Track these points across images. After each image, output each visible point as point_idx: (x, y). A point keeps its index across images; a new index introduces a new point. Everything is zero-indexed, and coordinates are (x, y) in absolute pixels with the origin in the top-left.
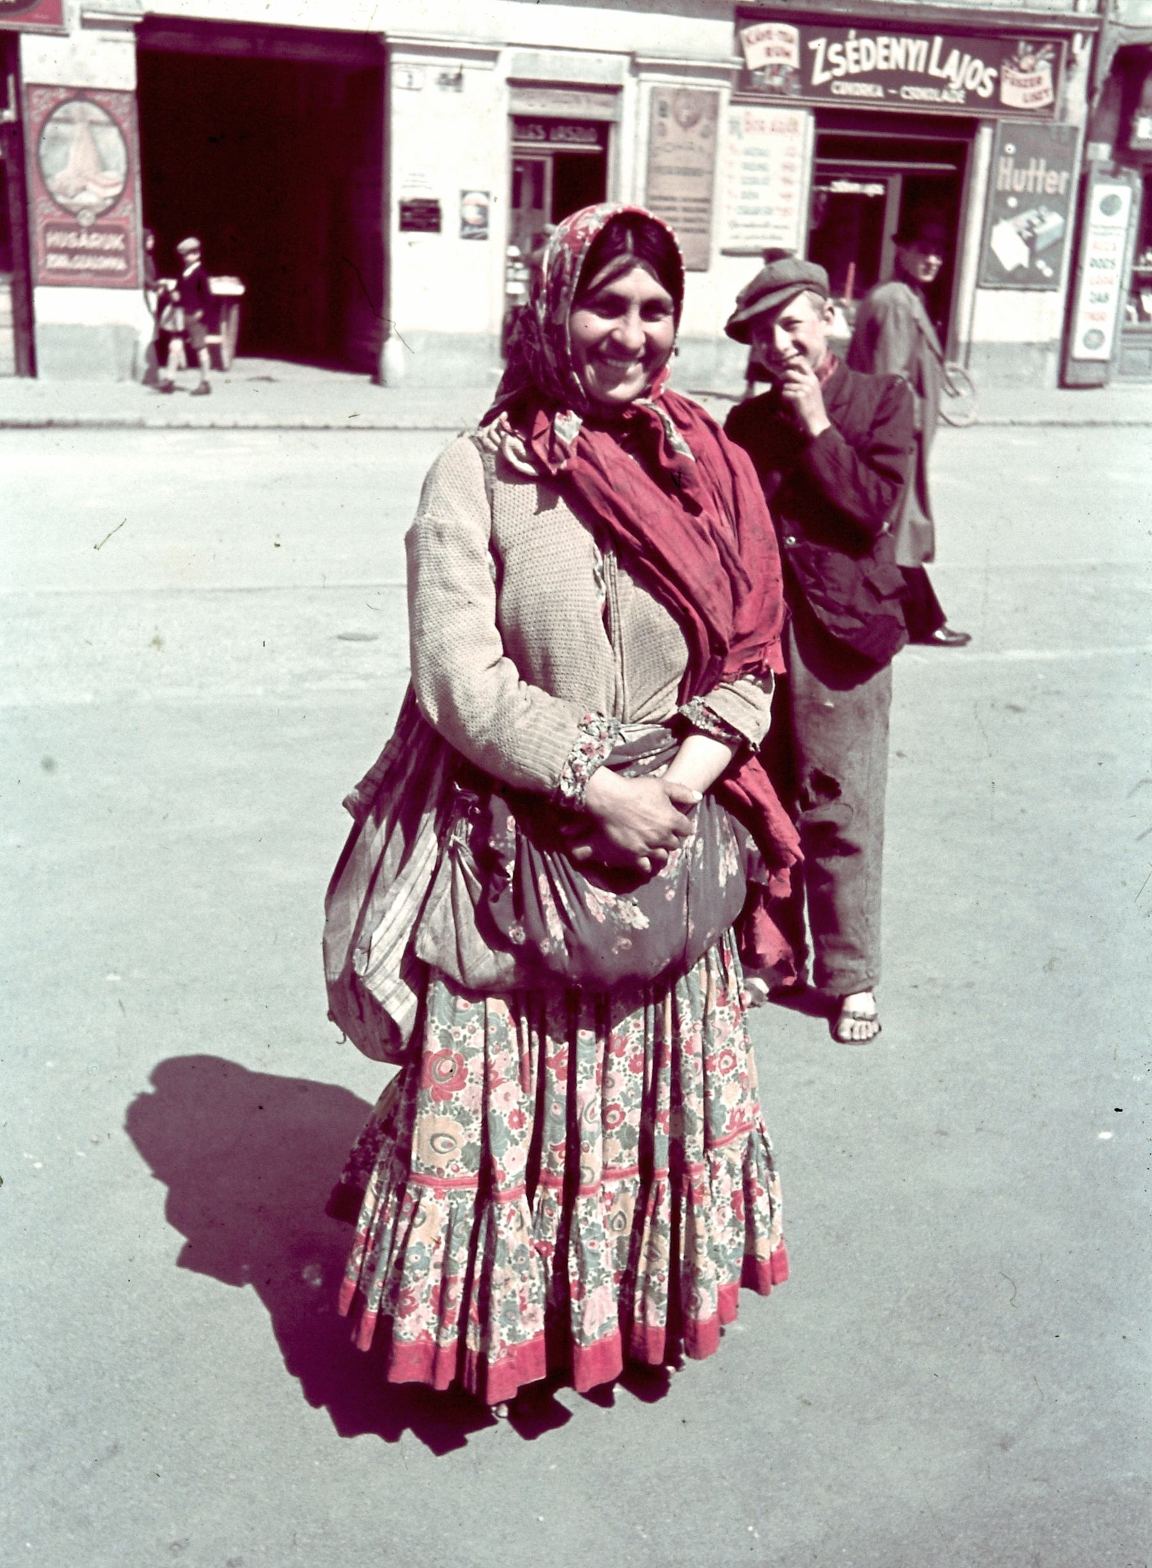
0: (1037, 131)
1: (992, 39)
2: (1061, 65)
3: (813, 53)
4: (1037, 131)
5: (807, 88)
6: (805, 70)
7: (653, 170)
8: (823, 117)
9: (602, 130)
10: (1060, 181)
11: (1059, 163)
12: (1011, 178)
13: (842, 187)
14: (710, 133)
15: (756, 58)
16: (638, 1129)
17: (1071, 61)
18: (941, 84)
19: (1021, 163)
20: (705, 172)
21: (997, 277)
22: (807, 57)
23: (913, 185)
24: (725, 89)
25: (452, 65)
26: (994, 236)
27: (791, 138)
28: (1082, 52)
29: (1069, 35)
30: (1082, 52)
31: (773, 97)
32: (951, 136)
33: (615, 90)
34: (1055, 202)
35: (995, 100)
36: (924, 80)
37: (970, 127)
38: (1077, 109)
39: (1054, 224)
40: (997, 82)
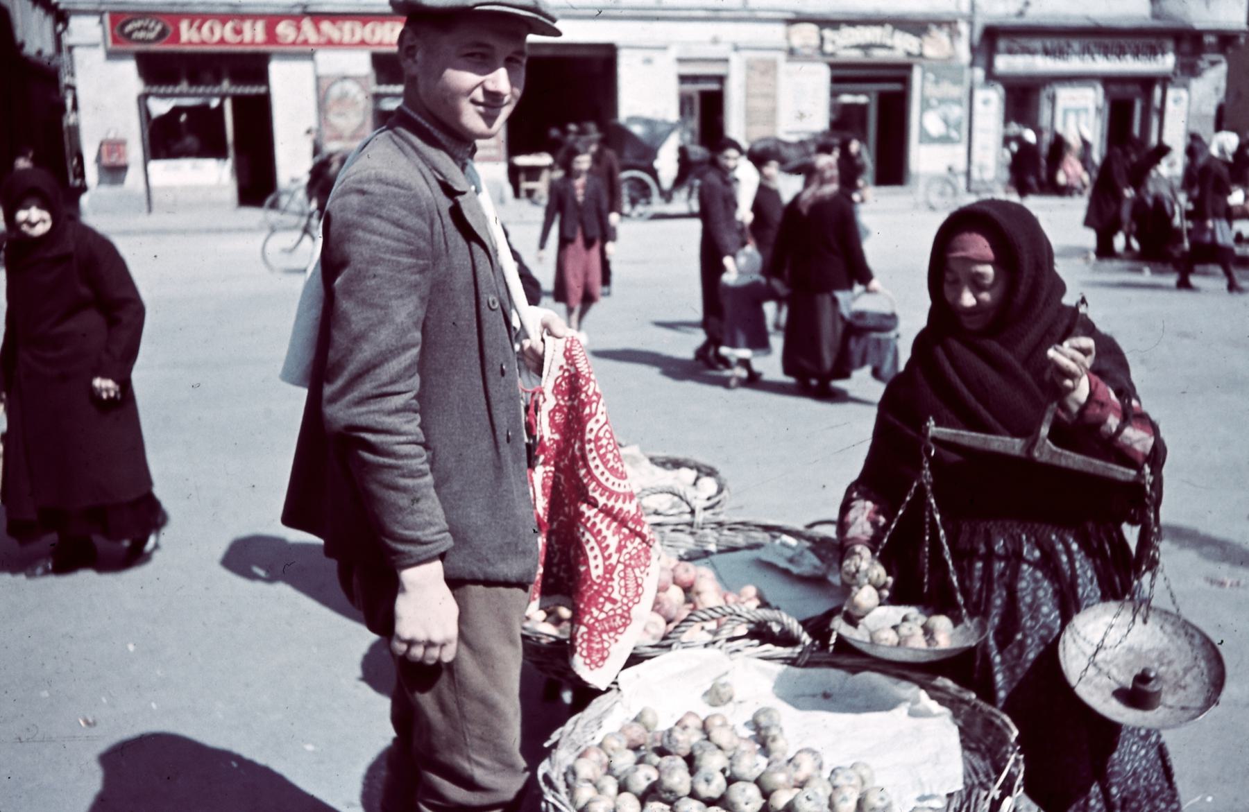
0: (944, 70)
1: (917, 26)
2: (954, 34)
3: (1153, 52)
4: (944, 70)
5: (823, 54)
6: (821, 47)
7: (748, 96)
8: (833, 66)
9: (721, 79)
10: (959, 91)
11: (957, 82)
12: (932, 91)
13: (847, 99)
14: (775, 77)
15: (797, 41)
16: (996, 586)
17: (959, 34)
18: (891, 48)
19: (937, 82)
20: (772, 97)
21: (926, 138)
22: (822, 39)
23: (884, 98)
24: (781, 57)
25: (648, 53)
26: (924, 120)
27: (821, 75)
28: (963, 28)
29: (956, 22)
30: (963, 28)
31: (808, 59)
32: (900, 73)
33: (726, 61)
34: (958, 102)
35: (921, 55)
36: (883, 46)
37: (908, 67)
38: (964, 54)
39: (958, 112)
40: (921, 46)
